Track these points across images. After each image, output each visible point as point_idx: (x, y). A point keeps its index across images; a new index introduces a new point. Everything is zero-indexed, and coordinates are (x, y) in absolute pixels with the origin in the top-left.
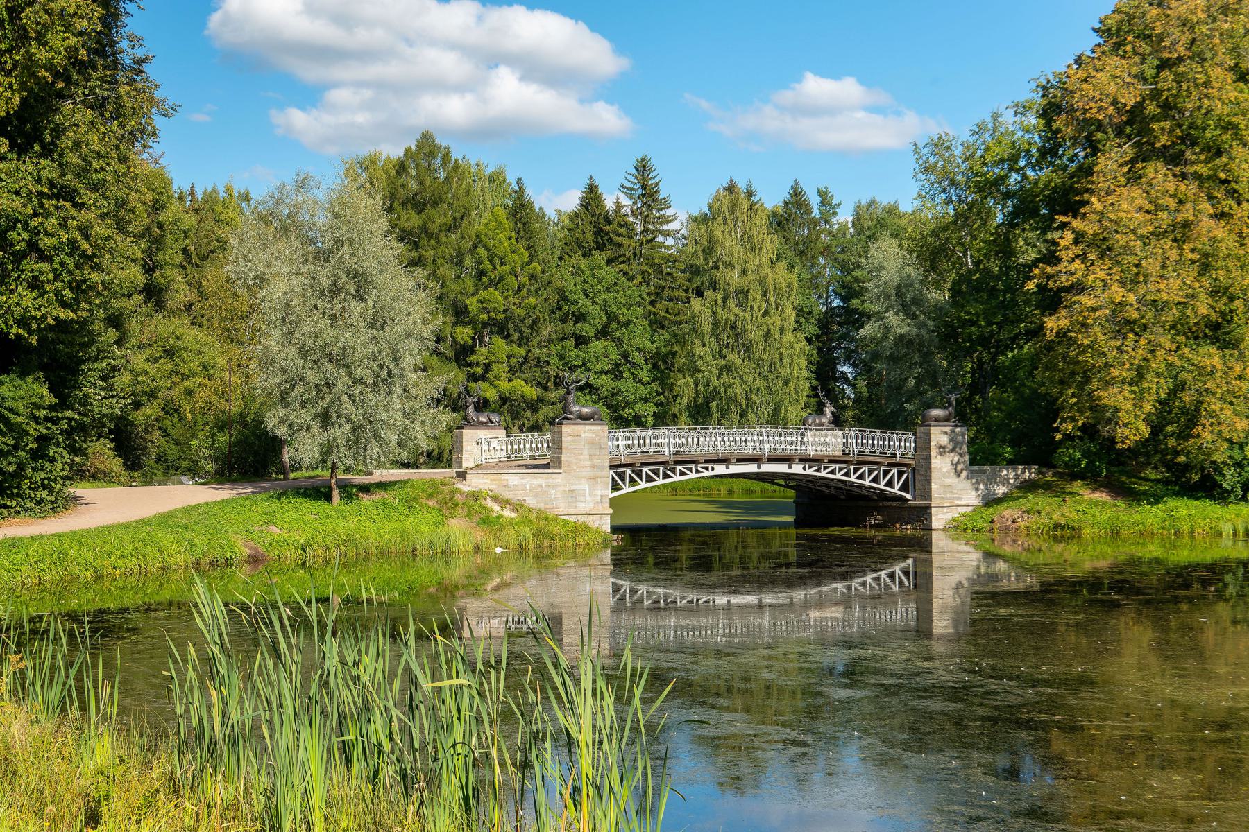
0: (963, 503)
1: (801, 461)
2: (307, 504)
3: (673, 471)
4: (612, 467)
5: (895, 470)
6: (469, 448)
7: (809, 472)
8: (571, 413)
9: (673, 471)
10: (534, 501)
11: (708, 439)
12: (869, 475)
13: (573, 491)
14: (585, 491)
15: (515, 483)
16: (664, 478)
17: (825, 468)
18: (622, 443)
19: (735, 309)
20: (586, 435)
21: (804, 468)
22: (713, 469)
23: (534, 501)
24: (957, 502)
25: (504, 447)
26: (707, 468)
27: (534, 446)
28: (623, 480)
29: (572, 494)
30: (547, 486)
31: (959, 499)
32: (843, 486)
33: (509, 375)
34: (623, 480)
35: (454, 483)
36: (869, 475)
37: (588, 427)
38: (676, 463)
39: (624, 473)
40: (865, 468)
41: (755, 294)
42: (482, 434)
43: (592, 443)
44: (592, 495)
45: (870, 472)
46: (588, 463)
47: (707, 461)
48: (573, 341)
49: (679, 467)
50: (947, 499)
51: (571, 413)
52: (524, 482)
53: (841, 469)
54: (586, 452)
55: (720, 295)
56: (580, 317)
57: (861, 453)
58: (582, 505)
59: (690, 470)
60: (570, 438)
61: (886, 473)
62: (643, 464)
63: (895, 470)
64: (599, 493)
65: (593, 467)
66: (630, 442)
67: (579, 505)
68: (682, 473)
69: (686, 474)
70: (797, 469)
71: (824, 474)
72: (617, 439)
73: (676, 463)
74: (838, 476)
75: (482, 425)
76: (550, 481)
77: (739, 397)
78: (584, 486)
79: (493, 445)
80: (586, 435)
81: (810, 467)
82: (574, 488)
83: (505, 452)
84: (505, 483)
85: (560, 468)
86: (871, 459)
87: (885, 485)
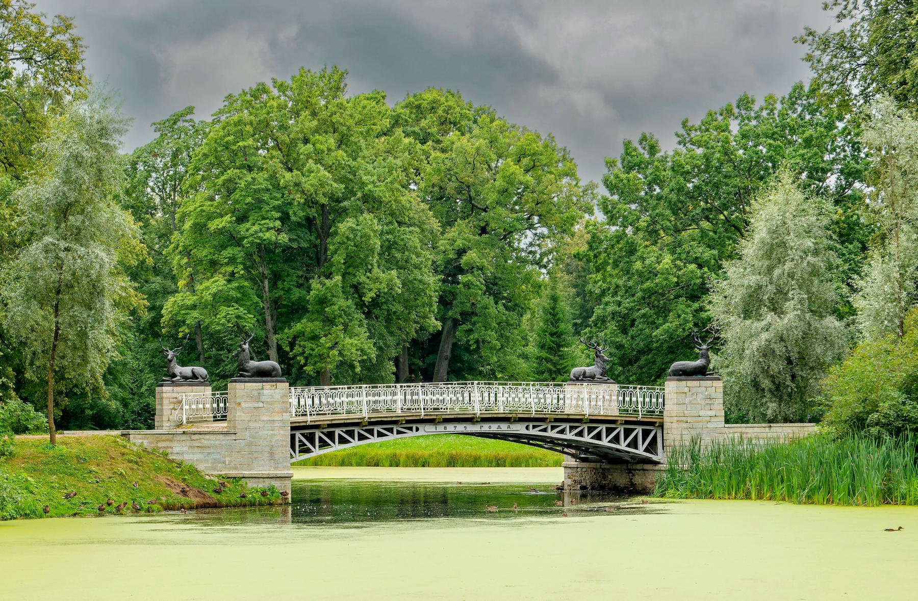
5: (639, 430)
16: (359, 439)
21: (527, 428)
28: (312, 442)
39: (313, 435)
59: (391, 430)
63: (639, 430)
81: (534, 427)
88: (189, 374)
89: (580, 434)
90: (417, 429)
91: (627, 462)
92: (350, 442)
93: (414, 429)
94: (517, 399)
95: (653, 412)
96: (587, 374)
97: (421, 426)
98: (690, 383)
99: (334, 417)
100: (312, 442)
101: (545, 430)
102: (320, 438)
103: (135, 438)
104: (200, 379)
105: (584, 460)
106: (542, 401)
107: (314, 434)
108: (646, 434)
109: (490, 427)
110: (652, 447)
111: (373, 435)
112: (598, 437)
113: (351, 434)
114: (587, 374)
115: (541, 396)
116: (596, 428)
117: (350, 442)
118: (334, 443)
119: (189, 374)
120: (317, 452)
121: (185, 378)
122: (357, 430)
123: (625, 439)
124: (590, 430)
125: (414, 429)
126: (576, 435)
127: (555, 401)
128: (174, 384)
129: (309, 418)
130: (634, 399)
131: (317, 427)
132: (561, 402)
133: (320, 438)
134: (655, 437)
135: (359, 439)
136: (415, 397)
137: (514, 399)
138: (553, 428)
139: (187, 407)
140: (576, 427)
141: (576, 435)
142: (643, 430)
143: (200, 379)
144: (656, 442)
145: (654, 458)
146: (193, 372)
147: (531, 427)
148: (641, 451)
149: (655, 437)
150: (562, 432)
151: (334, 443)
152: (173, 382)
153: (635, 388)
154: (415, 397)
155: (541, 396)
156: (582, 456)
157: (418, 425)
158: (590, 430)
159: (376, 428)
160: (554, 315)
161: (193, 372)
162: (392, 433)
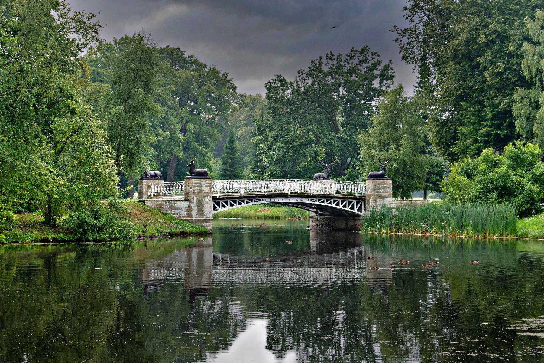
3: (243, 201)
26: (260, 200)
28: (219, 205)
57: (337, 193)
59: (252, 201)
81: (311, 200)
88: (154, 174)
89: (330, 203)
90: (263, 200)
91: (346, 216)
95: (339, 192)
96: (321, 176)
98: (378, 181)
99: (230, 194)
100: (219, 205)
101: (323, 202)
102: (222, 204)
103: (147, 203)
105: (320, 215)
106: (292, 187)
107: (219, 202)
109: (293, 200)
110: (360, 209)
111: (236, 204)
112: (338, 204)
113: (235, 202)
114: (321, 176)
115: (292, 185)
116: (337, 200)
118: (228, 206)
119: (154, 174)
121: (152, 176)
123: (349, 205)
124: (342, 202)
128: (147, 179)
129: (218, 195)
130: (353, 188)
131: (221, 199)
133: (222, 204)
138: (319, 200)
139: (154, 189)
140: (329, 200)
142: (356, 202)
143: (159, 177)
145: (362, 214)
148: (355, 211)
153: (354, 183)
155: (292, 185)
156: (320, 213)
157: (263, 199)
158: (342, 202)
159: (246, 200)
160: (232, 149)
162: (252, 202)
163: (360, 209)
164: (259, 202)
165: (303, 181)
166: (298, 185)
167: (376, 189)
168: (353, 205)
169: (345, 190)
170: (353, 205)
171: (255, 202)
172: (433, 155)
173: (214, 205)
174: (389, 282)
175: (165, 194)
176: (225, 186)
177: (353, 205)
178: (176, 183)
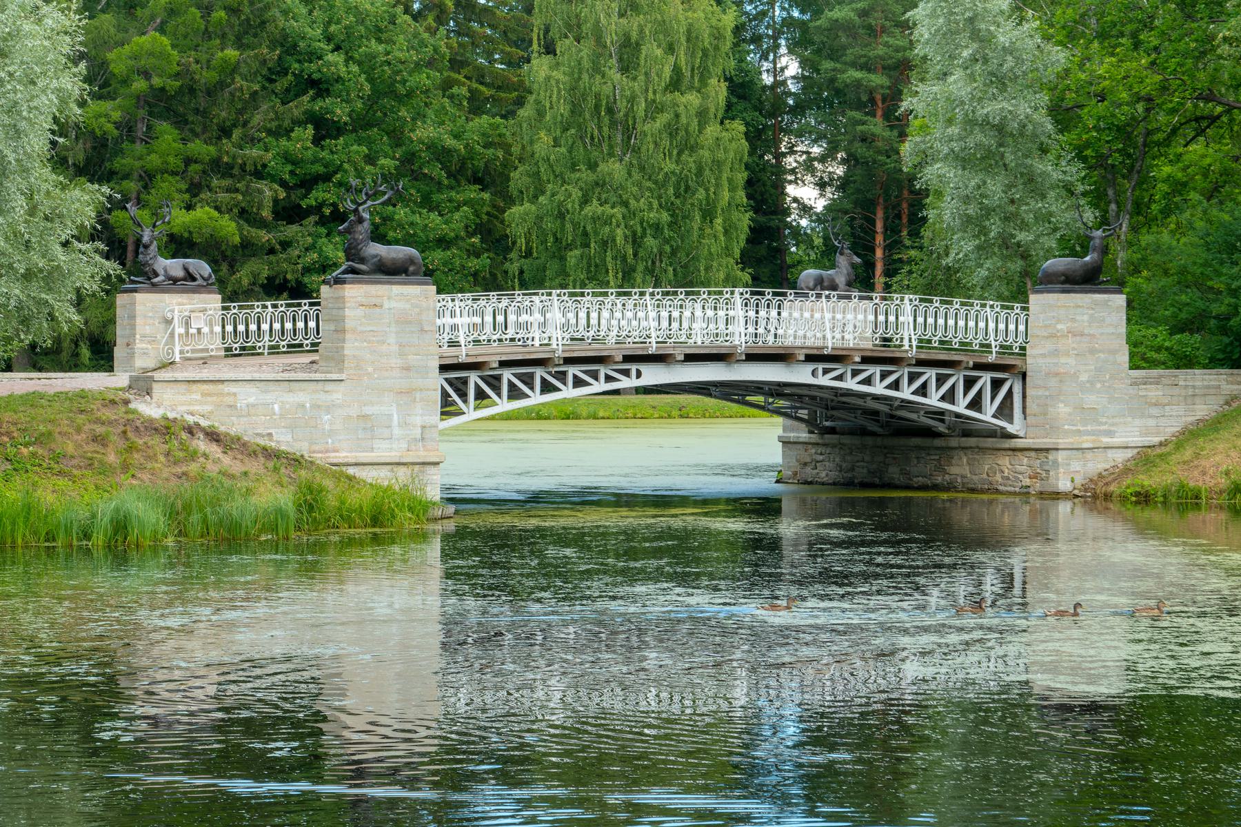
0: (1117, 441)
1: (810, 358)
2: (1028, 379)
3: (562, 376)
4: (444, 368)
5: (986, 378)
6: (148, 330)
7: (825, 381)
8: (362, 260)
9: (562, 376)
10: (289, 438)
11: (618, 315)
12: (938, 387)
13: (366, 417)
14: (390, 416)
15: (252, 400)
16: (510, 397)
17: (855, 373)
18: (463, 321)
19: (616, 76)
20: (393, 304)
21: (814, 373)
22: (639, 374)
23: (289, 438)
24: (1106, 440)
25: (218, 329)
26: (626, 373)
27: (277, 326)
28: (463, 395)
29: (367, 425)
30: (316, 407)
31: (1110, 433)
32: (883, 408)
33: (187, 196)
34: (463, 395)
35: (127, 402)
36: (938, 387)
37: (397, 289)
38: (569, 361)
39: (465, 381)
40: (931, 374)
41: (652, 50)
42: (176, 304)
43: (403, 321)
44: (404, 424)
45: (941, 380)
46: (396, 362)
47: (628, 359)
48: (310, 130)
49: (572, 370)
50: (1088, 433)
51: (362, 260)
52: (269, 398)
53: (884, 376)
54: (392, 339)
55: (586, 50)
56: (319, 86)
57: (924, 343)
58: (384, 445)
59: (595, 376)
60: (360, 312)
61: (969, 383)
62: (504, 364)
63: (986, 378)
64: (418, 421)
65: (407, 369)
66: (478, 320)
67: (377, 444)
68: (578, 383)
69: (585, 384)
70: (801, 375)
71: (851, 384)
72: (453, 315)
73: (569, 361)
74: (879, 388)
75: (175, 284)
76: (323, 396)
77: (619, 240)
78: (388, 408)
79: (195, 325)
80: (393, 304)
81: (826, 372)
82: (368, 410)
83: (219, 340)
84: (229, 400)
85: (341, 371)
86: (943, 356)
87: (967, 407)
92: (559, 390)
93: (634, 373)
94: (635, 323)
97: (644, 368)
101: (840, 378)
104: (200, 282)
108: (997, 384)
110: (1005, 410)
117: (559, 390)
118: (499, 395)
119: (180, 273)
120: (536, 398)
122: (539, 373)
124: (912, 378)
125: (634, 373)
126: (888, 387)
127: (665, 324)
128: (155, 288)
132: (675, 325)
134: (1010, 393)
135: (510, 397)
136: (524, 318)
137: (629, 321)
141: (888, 387)
143: (200, 282)
144: (1012, 403)
145: (1011, 429)
146: (186, 269)
147: (820, 372)
148: (987, 415)
149: (1010, 393)
150: (868, 381)
151: (499, 395)
152: (154, 285)
153: (983, 306)
154: (524, 318)
158: (912, 378)
161: (186, 269)
162: (596, 379)
163: (1005, 410)
164: (625, 383)
165: (687, 294)
166: (665, 314)
167: (339, 308)
168: (953, 388)
169: (1011, 339)
170: (979, 393)
171: (609, 379)
172: (796, 152)
173: (445, 395)
174: (431, 732)
175: (227, 349)
176: (603, 322)
177: (953, 388)
178: (274, 306)
